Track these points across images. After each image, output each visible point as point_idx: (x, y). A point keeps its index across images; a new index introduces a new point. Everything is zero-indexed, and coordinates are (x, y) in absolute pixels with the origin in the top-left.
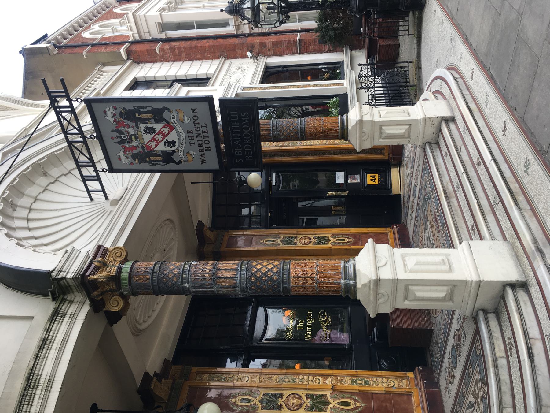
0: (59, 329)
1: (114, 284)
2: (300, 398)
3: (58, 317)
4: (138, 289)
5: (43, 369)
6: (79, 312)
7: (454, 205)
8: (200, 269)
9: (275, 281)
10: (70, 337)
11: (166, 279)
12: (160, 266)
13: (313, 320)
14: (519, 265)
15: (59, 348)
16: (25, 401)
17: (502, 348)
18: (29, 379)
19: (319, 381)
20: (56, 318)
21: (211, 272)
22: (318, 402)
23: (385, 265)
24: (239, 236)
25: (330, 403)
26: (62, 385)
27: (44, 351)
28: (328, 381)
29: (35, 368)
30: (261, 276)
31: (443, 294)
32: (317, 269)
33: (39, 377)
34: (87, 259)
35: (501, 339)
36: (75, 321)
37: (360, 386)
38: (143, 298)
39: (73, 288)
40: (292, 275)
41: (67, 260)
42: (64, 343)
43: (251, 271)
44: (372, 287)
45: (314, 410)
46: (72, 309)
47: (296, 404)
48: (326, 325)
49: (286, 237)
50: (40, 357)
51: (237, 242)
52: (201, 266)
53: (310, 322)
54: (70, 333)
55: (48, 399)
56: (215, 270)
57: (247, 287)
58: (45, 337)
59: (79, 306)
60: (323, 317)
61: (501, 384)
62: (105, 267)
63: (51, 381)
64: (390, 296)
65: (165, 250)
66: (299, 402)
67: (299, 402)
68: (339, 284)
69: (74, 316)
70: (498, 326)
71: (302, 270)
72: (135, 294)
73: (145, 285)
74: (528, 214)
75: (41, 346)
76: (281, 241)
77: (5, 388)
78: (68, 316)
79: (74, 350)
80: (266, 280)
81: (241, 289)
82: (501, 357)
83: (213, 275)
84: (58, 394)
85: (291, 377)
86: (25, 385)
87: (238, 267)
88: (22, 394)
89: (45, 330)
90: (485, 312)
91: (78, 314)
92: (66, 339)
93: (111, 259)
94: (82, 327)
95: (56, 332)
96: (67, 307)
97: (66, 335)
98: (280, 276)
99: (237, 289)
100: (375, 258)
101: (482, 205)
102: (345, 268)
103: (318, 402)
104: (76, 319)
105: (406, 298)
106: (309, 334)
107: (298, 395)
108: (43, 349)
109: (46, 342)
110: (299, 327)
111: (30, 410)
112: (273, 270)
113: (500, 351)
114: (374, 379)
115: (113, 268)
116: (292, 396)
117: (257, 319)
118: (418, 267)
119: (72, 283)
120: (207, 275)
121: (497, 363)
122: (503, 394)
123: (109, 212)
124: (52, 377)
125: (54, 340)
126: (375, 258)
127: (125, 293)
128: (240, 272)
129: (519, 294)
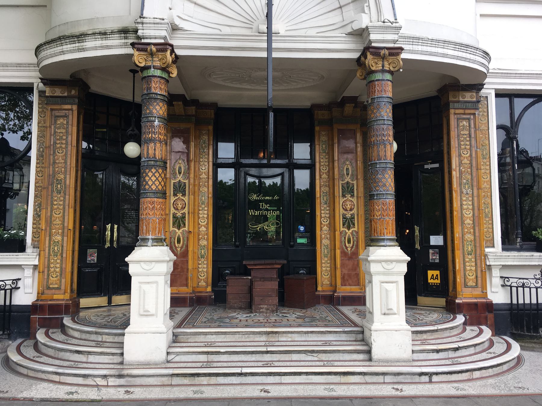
0: (116, 39)
2: (183, 208)
3: (123, 35)
7: (257, 337)
20: (122, 34)
21: (153, 138)
25: (179, 230)
27: (99, 37)
28: (203, 229)
41: (154, 23)
43: (147, 168)
48: (265, 227)
49: (353, 186)
51: (347, 139)
52: (152, 129)
53: (267, 213)
58: (107, 33)
62: (151, 56)
63: (83, 50)
64: (150, 271)
66: (179, 209)
67: (349, 209)
69: (125, 45)
74: (165, 380)
76: (348, 183)
84: (78, 58)
85: (206, 201)
86: (77, 35)
87: (150, 158)
89: (112, 31)
93: (160, 57)
94: (119, 54)
95: (113, 38)
100: (143, 261)
101: (221, 355)
102: (148, 239)
103: (179, 221)
106: (255, 213)
107: (185, 208)
109: (105, 35)
110: (262, 205)
112: (147, 185)
113: (106, 338)
114: (205, 262)
115: (151, 62)
116: (184, 203)
117: (269, 169)
121: (99, 334)
123: (251, 26)
126: (143, 261)
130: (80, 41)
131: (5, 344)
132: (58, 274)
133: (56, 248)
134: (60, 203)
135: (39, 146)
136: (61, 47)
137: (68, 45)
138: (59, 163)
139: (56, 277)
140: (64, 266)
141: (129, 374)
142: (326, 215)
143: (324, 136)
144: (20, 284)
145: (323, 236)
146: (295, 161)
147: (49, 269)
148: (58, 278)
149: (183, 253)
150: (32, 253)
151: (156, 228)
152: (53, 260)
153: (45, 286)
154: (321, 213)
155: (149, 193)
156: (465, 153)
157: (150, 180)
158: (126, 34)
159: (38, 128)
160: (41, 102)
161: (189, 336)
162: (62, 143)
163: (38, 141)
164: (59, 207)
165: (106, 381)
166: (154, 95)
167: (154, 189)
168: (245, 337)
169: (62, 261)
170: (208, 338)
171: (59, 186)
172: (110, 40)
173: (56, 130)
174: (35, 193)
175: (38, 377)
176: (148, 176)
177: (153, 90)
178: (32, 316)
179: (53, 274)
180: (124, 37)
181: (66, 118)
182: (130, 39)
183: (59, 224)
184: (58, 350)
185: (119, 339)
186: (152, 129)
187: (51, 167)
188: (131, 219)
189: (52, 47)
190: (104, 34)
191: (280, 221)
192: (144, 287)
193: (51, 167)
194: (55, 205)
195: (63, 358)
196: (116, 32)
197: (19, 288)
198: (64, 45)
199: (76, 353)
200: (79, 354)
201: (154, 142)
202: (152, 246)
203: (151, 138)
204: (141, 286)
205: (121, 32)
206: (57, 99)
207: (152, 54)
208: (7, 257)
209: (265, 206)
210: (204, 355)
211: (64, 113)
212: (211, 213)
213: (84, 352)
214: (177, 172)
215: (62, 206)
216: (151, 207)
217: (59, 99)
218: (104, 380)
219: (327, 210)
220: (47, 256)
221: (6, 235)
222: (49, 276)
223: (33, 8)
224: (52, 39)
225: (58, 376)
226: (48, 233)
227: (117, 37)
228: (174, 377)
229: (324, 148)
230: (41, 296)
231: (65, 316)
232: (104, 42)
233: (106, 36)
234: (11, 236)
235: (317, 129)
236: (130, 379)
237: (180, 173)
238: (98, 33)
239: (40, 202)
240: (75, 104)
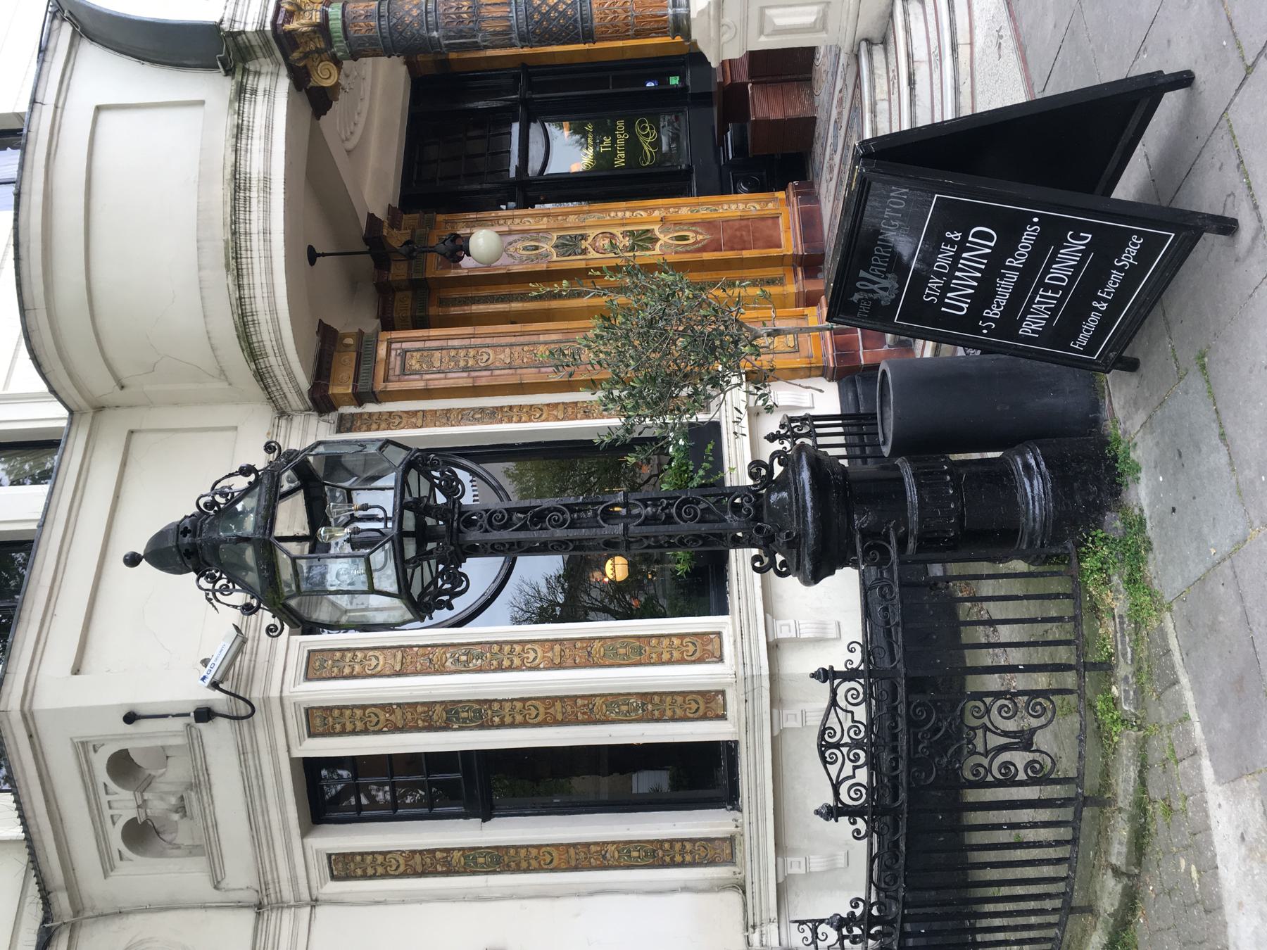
1: (321, 39)
3: (247, 95)
4: (359, 45)
8: (451, 7)
9: (571, 18)
12: (388, 6)
17: (886, 88)
18: (235, 179)
21: (470, 10)
27: (244, 141)
28: (657, 213)
30: (548, 11)
31: (811, 19)
33: (248, 175)
37: (704, 214)
39: (257, 50)
44: (712, 13)
46: (263, 83)
57: (528, 31)
60: (644, 129)
62: (302, 13)
63: (267, 180)
64: (738, 28)
68: (665, 15)
69: (269, 93)
70: (884, 60)
72: (355, 56)
73: (370, 37)
75: (237, 135)
77: (199, 197)
78: (260, 93)
80: (557, 17)
81: (519, 35)
84: (283, 196)
90: (870, 42)
95: (251, 116)
99: (513, 36)
105: (761, 32)
107: (611, 234)
109: (242, 130)
110: (603, 147)
113: (882, 92)
116: (601, 235)
119: (255, 41)
120: (465, 16)
127: (340, 54)
130: (248, 185)
136: (254, 237)
155: (581, 12)
163: (459, 424)
172: (253, 122)
178: (863, 363)
180: (251, 95)
189: (250, 266)
190: (239, 131)
196: (239, 107)
205: (240, 96)
206: (362, 371)
208: (757, 896)
211: (396, 359)
212: (623, 204)
214: (534, 252)
223: (128, 464)
225: (960, 50)
232: (256, 134)
233: (245, 127)
237: (537, 248)
238: (237, 142)
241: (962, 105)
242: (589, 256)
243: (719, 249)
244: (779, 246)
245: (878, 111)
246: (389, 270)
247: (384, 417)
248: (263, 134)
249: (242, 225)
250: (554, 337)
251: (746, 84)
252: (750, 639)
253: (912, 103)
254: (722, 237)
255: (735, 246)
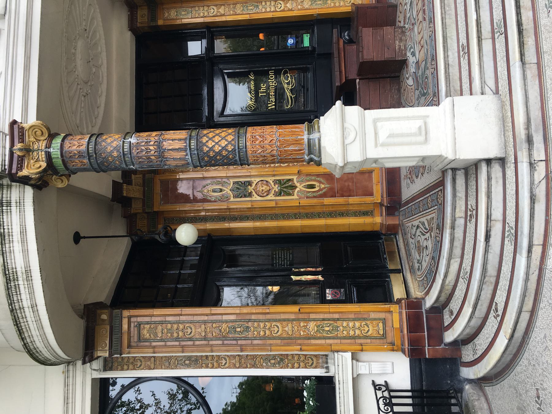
0: (11, 220)
3: (4, 208)
5: (15, 263)
6: (24, 198)
9: (232, 160)
10: (26, 227)
11: (106, 162)
13: (275, 83)
14: (503, 133)
15: (21, 241)
16: (12, 293)
17: (463, 208)
18: (6, 275)
19: (281, 5)
21: (156, 143)
22: (285, 187)
23: (354, 141)
24: (182, 180)
25: (297, 187)
26: (41, 273)
27: (7, 245)
29: (6, 263)
32: (278, 145)
34: (4, 142)
35: (465, 199)
36: (24, 209)
38: (82, 106)
40: (249, 152)
42: (23, 234)
43: (202, 150)
45: (282, 195)
47: (265, 190)
48: (290, 88)
50: (6, 252)
52: (143, 146)
53: (272, 86)
54: (25, 223)
55: (33, 286)
56: (159, 145)
59: (20, 190)
61: (455, 241)
62: (31, 153)
63: (28, 272)
64: (358, 130)
65: (86, 30)
66: (268, 188)
69: (20, 204)
70: (464, 184)
71: (260, 136)
74: (532, 71)
78: (13, 204)
79: (37, 240)
82: (460, 217)
83: (160, 157)
84: (41, 281)
86: (5, 281)
87: (186, 146)
88: (6, 288)
91: (24, 200)
92: (23, 230)
93: (32, 139)
94: (34, 215)
95: (10, 224)
96: (7, 193)
97: (21, 227)
98: (236, 155)
100: (344, 139)
101: (481, 21)
102: (309, 140)
103: (285, 187)
104: (24, 206)
106: (272, 102)
107: (267, 182)
108: (5, 244)
109: (4, 237)
111: (21, 298)
115: (40, 153)
116: (260, 182)
118: (391, 140)
121: (454, 223)
122: (454, 249)
124: (27, 268)
125: (12, 233)
126: (344, 139)
128: (190, 152)
129: (493, 169)
130: (16, 277)
131: (470, 393)
132: (364, 323)
133: (327, 329)
134: (262, 327)
135: (182, 365)
136: (26, 310)
137: (22, 298)
138: (205, 332)
139: (368, 326)
140: (352, 316)
141: (526, 127)
142: (272, 4)
143: (170, 14)
144: (380, 381)
145: (299, 7)
146: (203, 52)
147: (356, 337)
148: (368, 323)
149: (327, 180)
150: (335, 365)
151: (292, 132)
152: (344, 332)
153: (382, 341)
154: (270, 12)
156: (212, 11)
157: (220, 143)
158: (2, 203)
159: (157, 368)
160: (119, 367)
161: (452, 89)
162: (177, 329)
163: (176, 367)
164: (267, 327)
165: (538, 164)
166: (90, 146)
167: (232, 137)
168: (448, 11)
169: (344, 320)
170: (452, 62)
171: (238, 330)
172: (12, 229)
173: (158, 338)
174: (250, 368)
175: (535, 288)
176: (214, 146)
177: (83, 148)
178: (427, 357)
179: (364, 330)
181: (142, 326)
182: (10, 198)
183: (293, 327)
184: (485, 277)
185: (460, 190)
186: (143, 146)
187: (211, 343)
188: (284, 263)
189: (27, 326)
191: (282, 70)
192: (382, 137)
193: (211, 343)
194: (265, 333)
195: (497, 266)
197: (386, 382)
198: (22, 305)
199: (489, 241)
200: (490, 237)
201: (162, 142)
202: (319, 132)
203: (155, 147)
204: (381, 142)
206: (114, 340)
207: (28, 151)
209: (262, 90)
210: (483, 45)
213: (487, 226)
215: (267, 323)
216: (261, 139)
217: (114, 337)
218: (537, 168)
219: (266, 4)
220: (339, 341)
221: (311, 402)
222: (367, 337)
224: (15, 325)
226: (306, 342)
227: (8, 218)
228: (526, 60)
229: (186, 13)
230: (397, 346)
231: (423, 308)
233: (6, 234)
234: (311, 397)
235: (160, 22)
236: (533, 127)
237: (221, 190)
239: (262, 360)
240: (121, 314)
241: (528, 287)
242: (253, 199)
243: (333, 196)
244: (371, 194)
245: (456, 225)
246: (131, 206)
247: (131, 361)
248: (20, 239)
249: (16, 304)
250: (233, 317)
251: (355, 80)
252: (344, 406)
253: (486, 251)
254: (336, 186)
255: (345, 194)
